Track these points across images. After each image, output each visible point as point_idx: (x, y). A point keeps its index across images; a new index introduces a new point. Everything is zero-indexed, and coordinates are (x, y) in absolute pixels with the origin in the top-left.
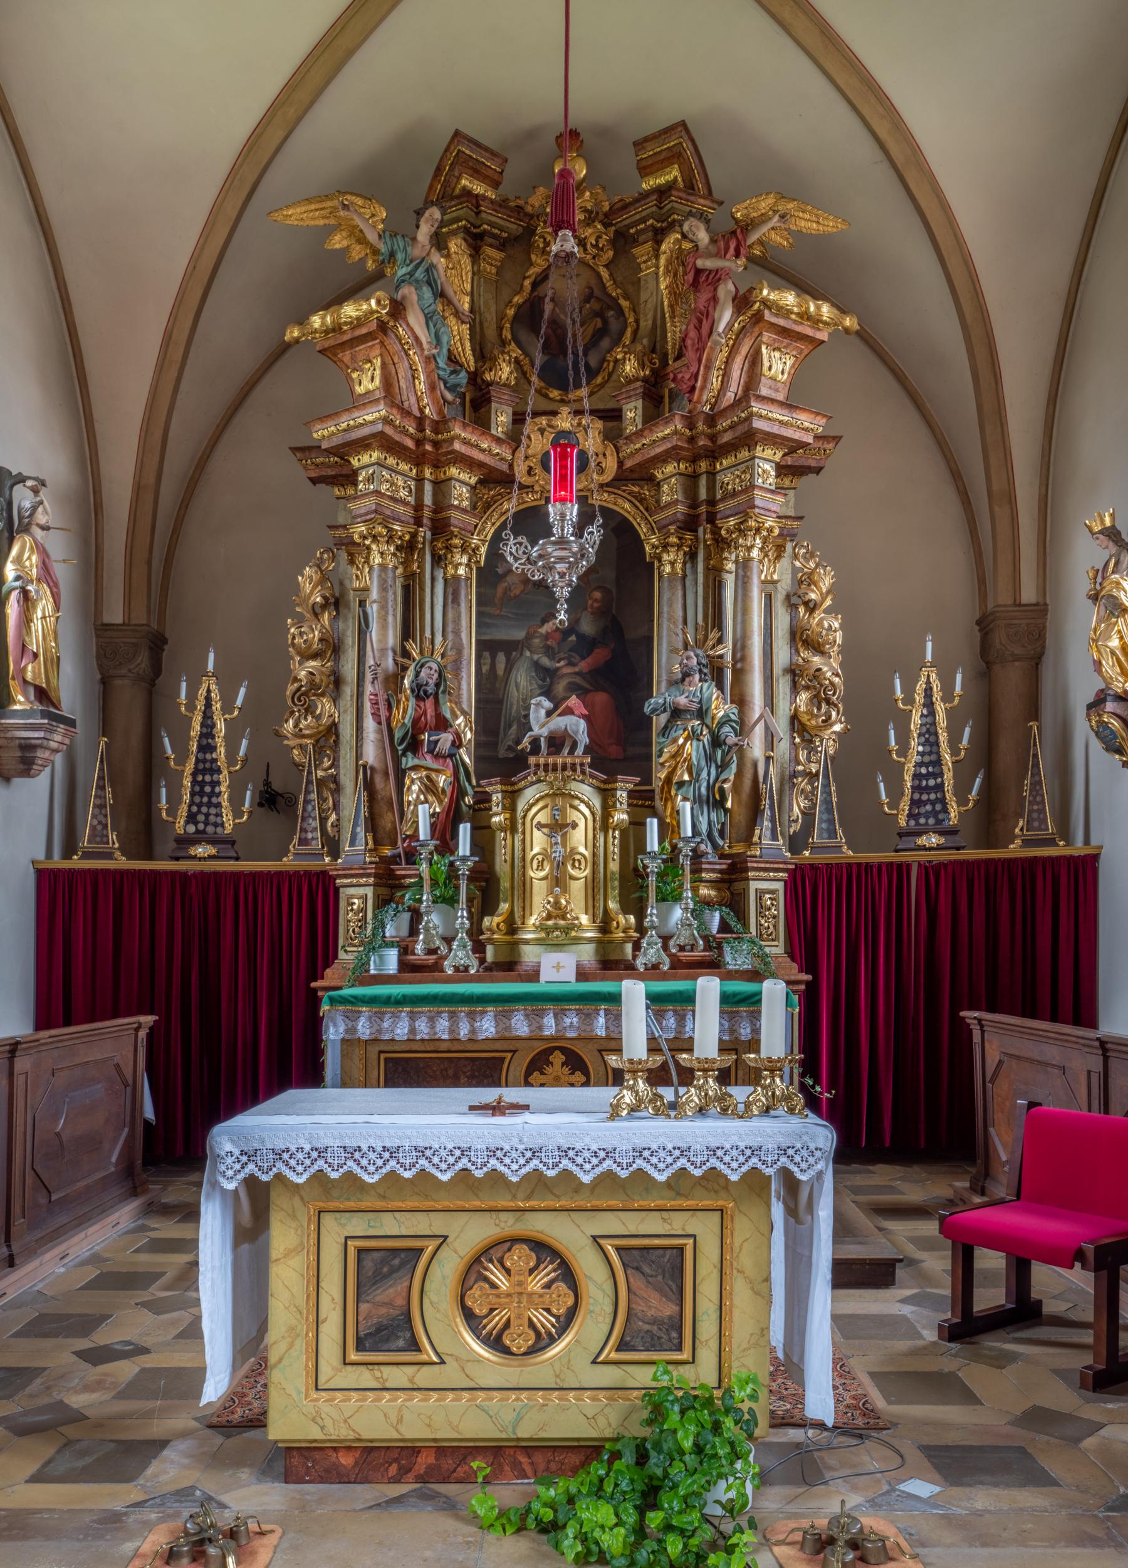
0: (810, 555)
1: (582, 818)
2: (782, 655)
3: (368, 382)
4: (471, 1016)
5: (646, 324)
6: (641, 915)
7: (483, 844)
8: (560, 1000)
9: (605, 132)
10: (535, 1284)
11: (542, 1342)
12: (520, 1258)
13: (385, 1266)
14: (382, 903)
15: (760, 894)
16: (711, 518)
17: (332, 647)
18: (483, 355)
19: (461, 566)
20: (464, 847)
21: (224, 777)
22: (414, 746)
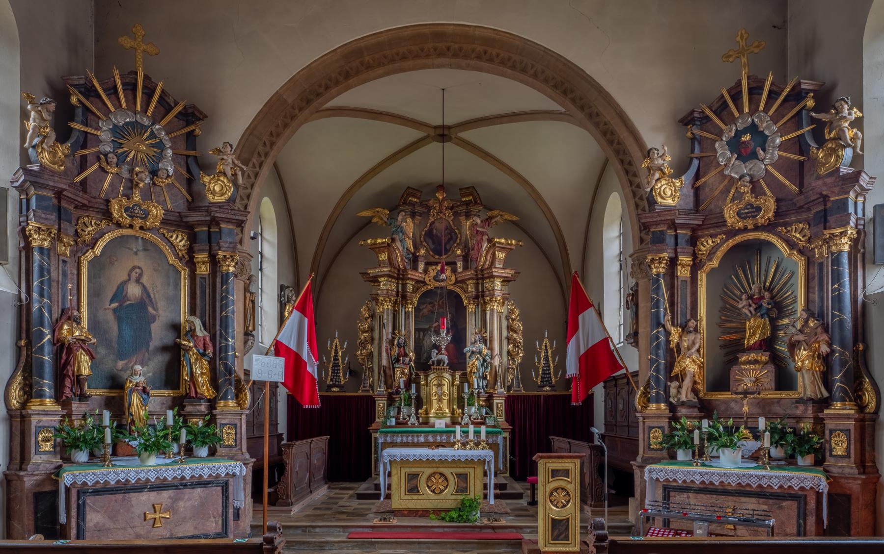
0: (512, 305)
1: (446, 383)
2: (505, 333)
3: (383, 257)
4: (418, 437)
5: (463, 238)
6: (463, 410)
7: (418, 390)
8: (441, 432)
10: (440, 481)
11: (442, 491)
12: (437, 476)
13: (413, 477)
14: (389, 405)
15: (497, 404)
16: (483, 296)
17: (371, 329)
18: (416, 247)
19: (410, 308)
20: (413, 391)
21: (341, 369)
22: (398, 361)
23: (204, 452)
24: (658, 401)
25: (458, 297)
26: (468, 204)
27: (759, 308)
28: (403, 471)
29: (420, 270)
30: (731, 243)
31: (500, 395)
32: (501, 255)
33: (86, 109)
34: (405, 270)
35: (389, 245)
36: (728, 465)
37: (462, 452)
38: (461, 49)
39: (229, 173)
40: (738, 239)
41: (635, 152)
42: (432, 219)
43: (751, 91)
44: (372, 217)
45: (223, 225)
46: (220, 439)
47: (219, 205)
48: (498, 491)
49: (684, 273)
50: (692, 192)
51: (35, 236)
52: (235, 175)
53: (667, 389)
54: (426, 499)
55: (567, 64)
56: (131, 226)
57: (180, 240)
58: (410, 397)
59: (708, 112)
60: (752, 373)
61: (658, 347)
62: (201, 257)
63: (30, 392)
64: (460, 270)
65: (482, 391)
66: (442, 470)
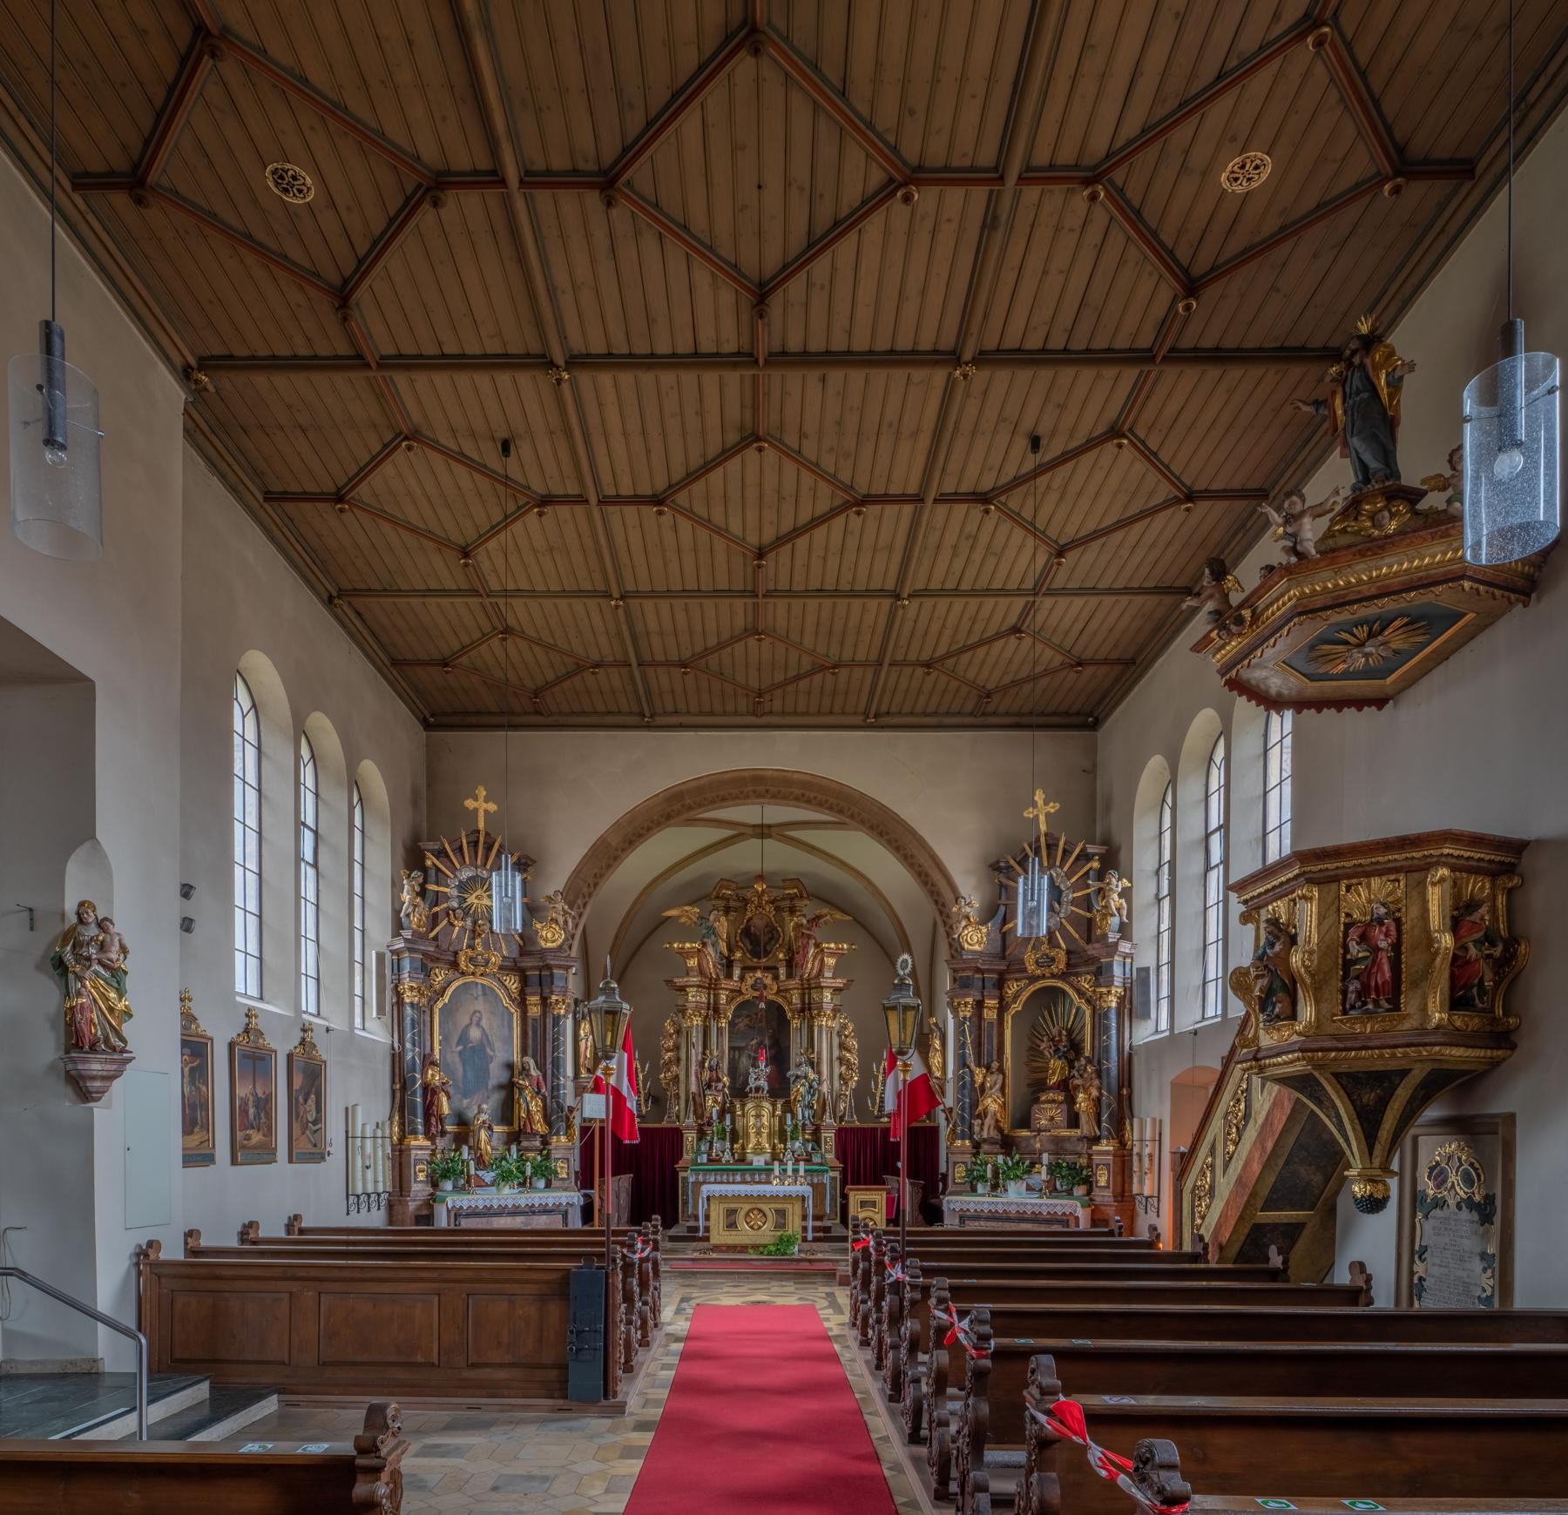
1: (765, 1113)
2: (836, 1053)
3: (693, 963)
7: (733, 1122)
9: (774, 874)
13: (731, 1213)
14: (699, 1139)
17: (677, 1048)
19: (724, 1023)
20: (728, 1122)
22: (709, 1087)
23: (541, 1184)
24: (963, 1138)
25: (780, 1008)
26: (792, 898)
27: (1057, 1050)
30: (1032, 988)
31: (829, 1127)
32: (831, 961)
33: (438, 869)
34: (718, 978)
36: (1016, 1196)
39: (561, 920)
40: (1038, 985)
41: (948, 895)
42: (749, 914)
43: (1049, 846)
46: (556, 1173)
47: (550, 950)
48: (818, 1223)
49: (990, 1015)
50: (999, 937)
52: (566, 922)
53: (971, 1127)
54: (744, 1234)
57: (513, 983)
59: (1012, 862)
60: (1048, 1114)
62: (533, 999)
63: (406, 1131)
64: (782, 977)
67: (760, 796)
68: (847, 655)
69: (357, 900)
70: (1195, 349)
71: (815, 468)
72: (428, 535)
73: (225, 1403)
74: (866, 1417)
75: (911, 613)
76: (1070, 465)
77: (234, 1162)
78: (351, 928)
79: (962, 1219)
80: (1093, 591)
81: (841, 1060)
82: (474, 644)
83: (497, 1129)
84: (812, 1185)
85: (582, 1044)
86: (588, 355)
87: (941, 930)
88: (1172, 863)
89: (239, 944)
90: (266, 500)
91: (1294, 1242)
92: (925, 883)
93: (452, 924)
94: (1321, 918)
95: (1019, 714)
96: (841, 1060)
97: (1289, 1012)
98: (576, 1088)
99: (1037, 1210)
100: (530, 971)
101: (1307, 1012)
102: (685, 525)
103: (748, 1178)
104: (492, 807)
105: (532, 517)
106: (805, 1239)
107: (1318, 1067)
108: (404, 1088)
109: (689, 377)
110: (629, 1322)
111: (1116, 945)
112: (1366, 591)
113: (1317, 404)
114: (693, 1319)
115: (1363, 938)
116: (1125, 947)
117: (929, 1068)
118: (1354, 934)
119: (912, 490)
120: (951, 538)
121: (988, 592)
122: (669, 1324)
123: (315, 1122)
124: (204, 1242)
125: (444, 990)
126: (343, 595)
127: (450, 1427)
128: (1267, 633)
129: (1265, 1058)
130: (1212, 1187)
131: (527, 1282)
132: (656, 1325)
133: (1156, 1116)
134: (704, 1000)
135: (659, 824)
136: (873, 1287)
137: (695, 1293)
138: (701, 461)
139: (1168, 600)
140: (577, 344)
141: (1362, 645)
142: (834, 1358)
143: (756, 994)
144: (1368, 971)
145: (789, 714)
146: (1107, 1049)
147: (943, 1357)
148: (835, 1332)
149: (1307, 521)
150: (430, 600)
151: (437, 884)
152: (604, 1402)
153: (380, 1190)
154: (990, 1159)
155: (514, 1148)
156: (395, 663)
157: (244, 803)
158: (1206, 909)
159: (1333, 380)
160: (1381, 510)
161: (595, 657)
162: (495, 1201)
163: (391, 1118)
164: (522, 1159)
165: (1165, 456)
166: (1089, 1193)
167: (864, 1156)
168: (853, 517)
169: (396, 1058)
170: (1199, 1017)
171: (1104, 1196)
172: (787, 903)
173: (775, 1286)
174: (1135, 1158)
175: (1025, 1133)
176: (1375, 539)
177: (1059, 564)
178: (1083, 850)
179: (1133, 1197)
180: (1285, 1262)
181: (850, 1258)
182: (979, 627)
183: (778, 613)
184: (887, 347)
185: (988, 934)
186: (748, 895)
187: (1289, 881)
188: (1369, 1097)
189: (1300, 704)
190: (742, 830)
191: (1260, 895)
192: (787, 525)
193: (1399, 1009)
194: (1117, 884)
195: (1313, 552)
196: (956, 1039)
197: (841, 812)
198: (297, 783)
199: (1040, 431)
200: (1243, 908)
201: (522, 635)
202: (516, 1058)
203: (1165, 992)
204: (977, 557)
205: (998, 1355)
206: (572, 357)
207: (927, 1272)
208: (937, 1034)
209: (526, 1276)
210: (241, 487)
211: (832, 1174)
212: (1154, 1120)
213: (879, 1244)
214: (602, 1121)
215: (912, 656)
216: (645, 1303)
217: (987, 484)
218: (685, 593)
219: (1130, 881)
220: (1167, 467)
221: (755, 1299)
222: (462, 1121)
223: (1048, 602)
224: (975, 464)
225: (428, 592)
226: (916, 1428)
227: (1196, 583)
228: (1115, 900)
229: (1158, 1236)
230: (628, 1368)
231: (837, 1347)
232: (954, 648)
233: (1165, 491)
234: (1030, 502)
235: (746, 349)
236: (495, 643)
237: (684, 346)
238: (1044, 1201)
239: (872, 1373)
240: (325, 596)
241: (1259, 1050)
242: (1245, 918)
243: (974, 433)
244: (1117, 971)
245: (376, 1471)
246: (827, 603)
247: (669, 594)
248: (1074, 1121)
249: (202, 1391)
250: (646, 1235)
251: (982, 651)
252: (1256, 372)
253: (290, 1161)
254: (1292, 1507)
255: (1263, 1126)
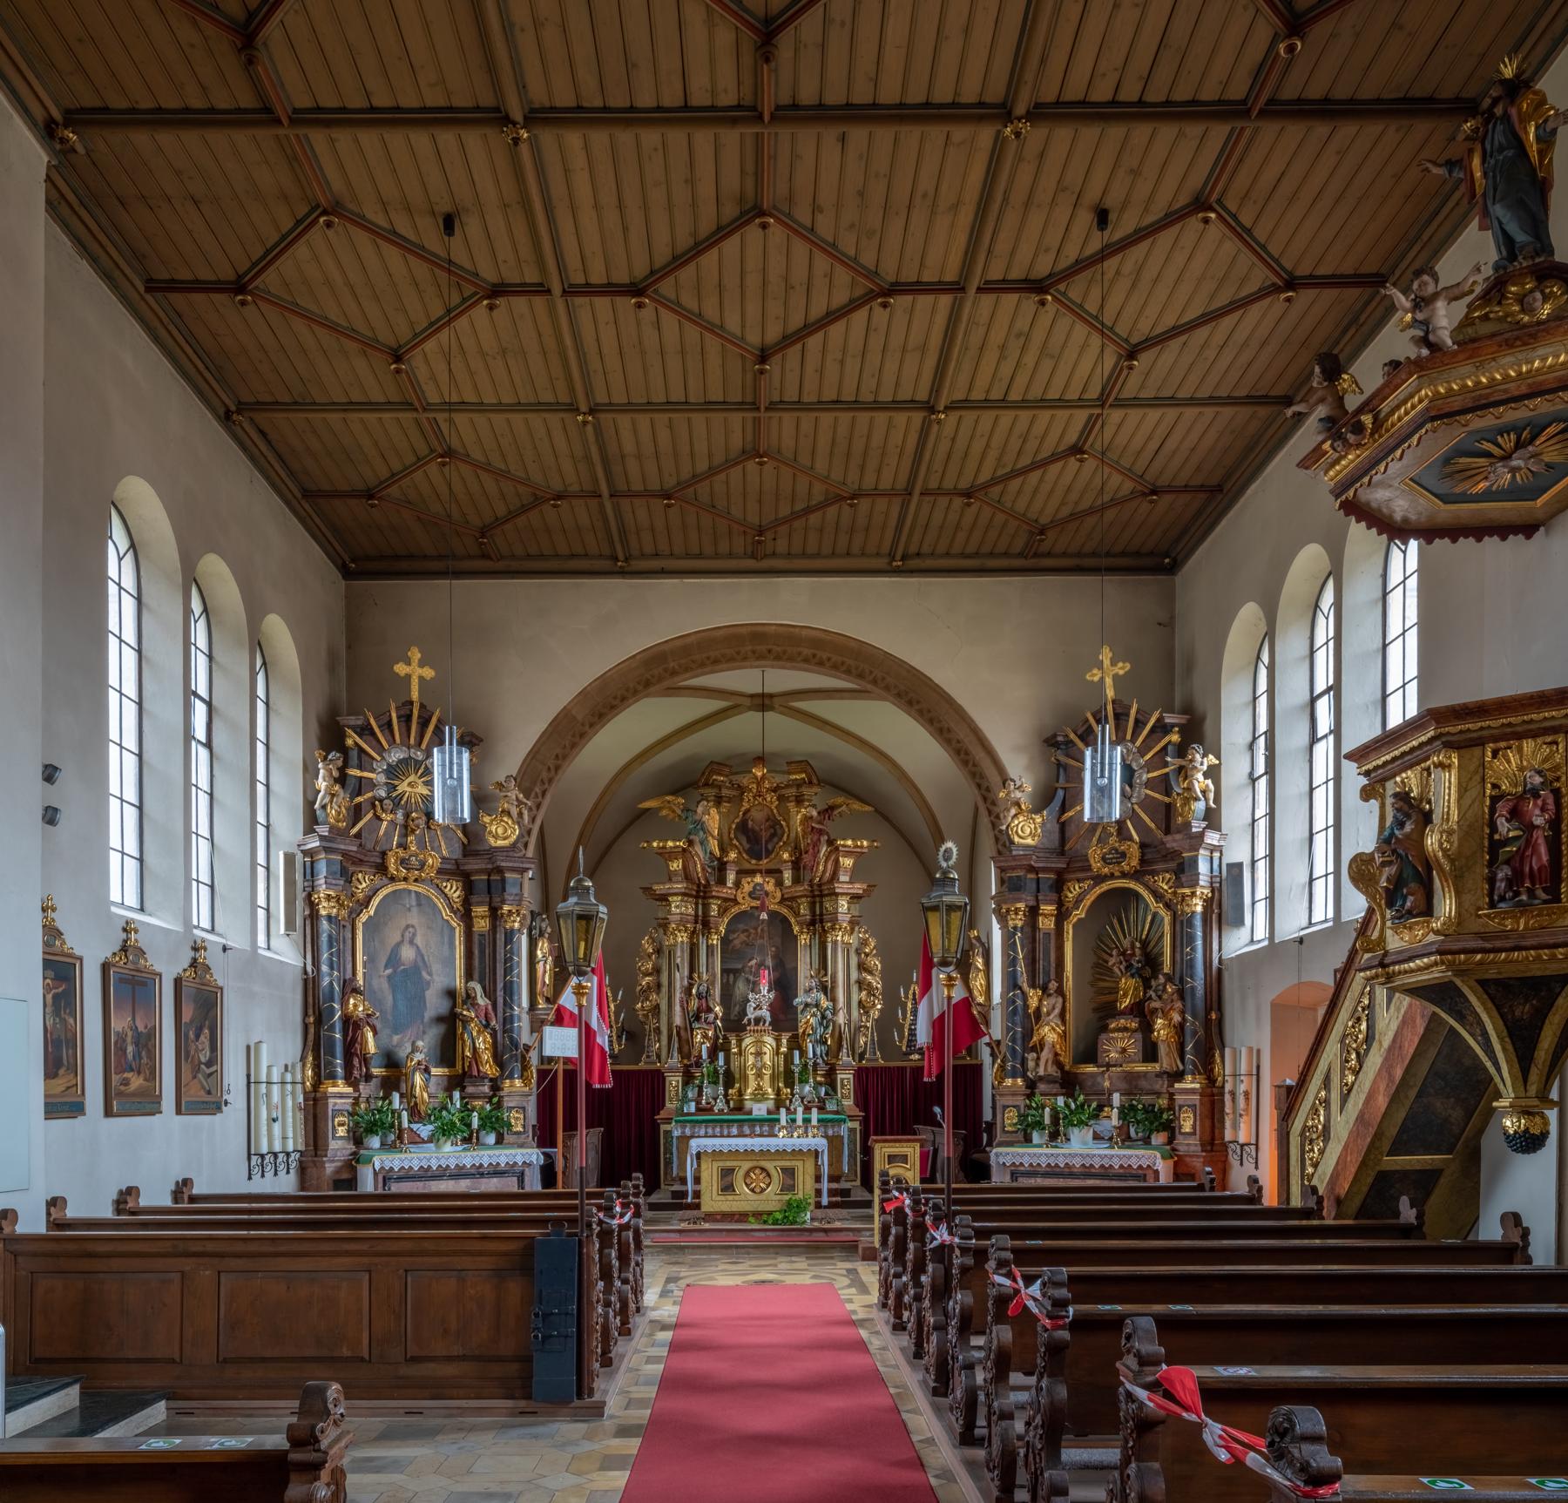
2: (854, 975)
3: (676, 865)
5: (793, 835)
7: (727, 1061)
9: (775, 755)
11: (763, 1190)
13: (727, 1173)
14: (686, 1083)
16: (822, 921)
17: (657, 971)
19: (715, 940)
20: (721, 1062)
22: (698, 1018)
24: (1014, 1076)
25: (785, 920)
26: (799, 784)
28: (716, 1165)
29: (730, 884)
30: (1098, 890)
31: (846, 1067)
32: (847, 862)
33: (361, 750)
34: (708, 885)
35: (684, 850)
36: (1081, 1147)
37: (788, 1141)
38: (785, 652)
39: (514, 811)
40: (1105, 887)
41: (994, 779)
42: (746, 806)
43: (1117, 716)
44: (660, 809)
45: (507, 875)
48: (835, 1186)
49: (1046, 923)
50: (1057, 827)
51: (325, 904)
52: (520, 814)
53: (1024, 1062)
54: (744, 1199)
55: (912, 670)
56: (405, 879)
57: (454, 891)
58: (716, 1071)
59: (1072, 736)
60: (1119, 1044)
61: (1015, 1012)
62: (480, 910)
63: (322, 1075)
64: (788, 883)
65: (820, 1061)
66: (763, 1164)
67: (761, 657)
68: (869, 482)
69: (261, 789)
70: (1299, 101)
71: (831, 250)
72: (350, 334)
73: (96, 1413)
74: (905, 1416)
75: (948, 429)
76: (1146, 244)
77: (108, 1113)
78: (254, 822)
79: (1014, 1175)
80: (1172, 402)
81: (861, 984)
82: (408, 471)
83: (435, 1071)
84: (826, 1136)
85: (540, 967)
86: (553, 109)
87: (985, 820)
88: (1270, 734)
89: (115, 841)
90: (148, 290)
91: (1428, 1194)
92: (965, 763)
93: (379, 818)
94: (1462, 790)
95: (1079, 555)
96: (861, 984)
97: (1423, 907)
98: (532, 1022)
99: (1106, 1163)
100: (476, 874)
101: (1446, 906)
102: (669, 320)
103: (747, 1130)
104: (428, 673)
105: (480, 312)
106: (818, 1205)
107: (1460, 973)
108: (319, 1022)
109: (677, 136)
110: (607, 1304)
111: (1201, 835)
112: (1514, 389)
113: (1450, 164)
114: (681, 1303)
115: (1515, 814)
116: (1212, 838)
117: (970, 990)
118: (1503, 809)
119: (950, 276)
120: (997, 337)
121: (1043, 404)
122: (654, 1309)
123: (209, 1064)
124: (71, 1213)
125: (368, 900)
126: (245, 410)
127: (386, 1436)
128: (1392, 442)
129: (1394, 963)
130: (1326, 1128)
131: (481, 1253)
132: (638, 1310)
133: (1254, 1047)
134: (691, 911)
135: (636, 692)
136: (910, 1256)
137: (683, 1271)
138: (691, 242)
139: (1263, 412)
140: (539, 97)
141: (1507, 457)
142: (861, 1346)
143: (756, 903)
144: (1521, 854)
145: (797, 556)
146: (1191, 964)
147: (1005, 1333)
148: (861, 1315)
149: (1440, 305)
150: (354, 416)
151: (360, 768)
152: (577, 1403)
153: (290, 1148)
154: (1047, 1100)
155: (457, 1095)
156: (307, 494)
157: (121, 666)
158: (1312, 790)
159: (1467, 138)
160: (1532, 291)
161: (557, 486)
162: (433, 1159)
163: (303, 1059)
164: (466, 1109)
165: (1261, 234)
166: (1171, 1140)
167: (893, 1098)
168: (878, 310)
169: (310, 984)
170: (1305, 923)
171: (1189, 1144)
172: (792, 791)
173: (783, 1263)
174: (1227, 1097)
175: (1091, 1069)
176: (1525, 326)
177: (1131, 368)
178: (1158, 720)
179: (1225, 1146)
180: (1420, 1216)
181: (877, 1225)
182: (1032, 445)
183: (784, 430)
184: (921, 99)
185: (1043, 824)
186: (745, 782)
187: (1421, 745)
188: (1523, 1010)
189: (1428, 533)
190: (740, 700)
191: (1386, 764)
192: (796, 321)
193: (1559, 900)
194: (1202, 762)
195: (1449, 342)
196: (1005, 954)
197: (861, 676)
198: (187, 643)
199: (1109, 203)
200: (1364, 781)
201: (466, 459)
202: (459, 983)
203: (1262, 892)
204: (1030, 359)
205: (1078, 1325)
206: (533, 111)
207: (982, 1234)
208: (979, 950)
209: (478, 1246)
210: (117, 274)
211: (850, 1124)
212: (1251, 1049)
213: (916, 1202)
214: (567, 1060)
215: (948, 484)
216: (625, 1281)
217: (1042, 269)
218: (669, 406)
219: (1218, 757)
220: (1263, 247)
221: (755, 1289)
222: (391, 1062)
223: (1116, 415)
224: (1031, 243)
225: (351, 406)
226: (969, 1425)
227: (1300, 392)
228: (1200, 781)
229: (1260, 1189)
230: (607, 1362)
231: (864, 1333)
232: (1000, 473)
233: (1261, 277)
234: (1096, 293)
235: (748, 101)
236: (433, 469)
237: (672, 98)
238: (1116, 1151)
239: (909, 1362)
240: (222, 411)
241: (1386, 954)
242: (1366, 794)
243: (1027, 205)
244: (1203, 867)
245: (313, 1468)
246: (845, 417)
247: (649, 407)
248: (1150, 1053)
249: (68, 1398)
250: (626, 1196)
251: (1034, 477)
252: (1373, 129)
253: (179, 1112)
254: (1467, 1487)
255: (1390, 1049)
